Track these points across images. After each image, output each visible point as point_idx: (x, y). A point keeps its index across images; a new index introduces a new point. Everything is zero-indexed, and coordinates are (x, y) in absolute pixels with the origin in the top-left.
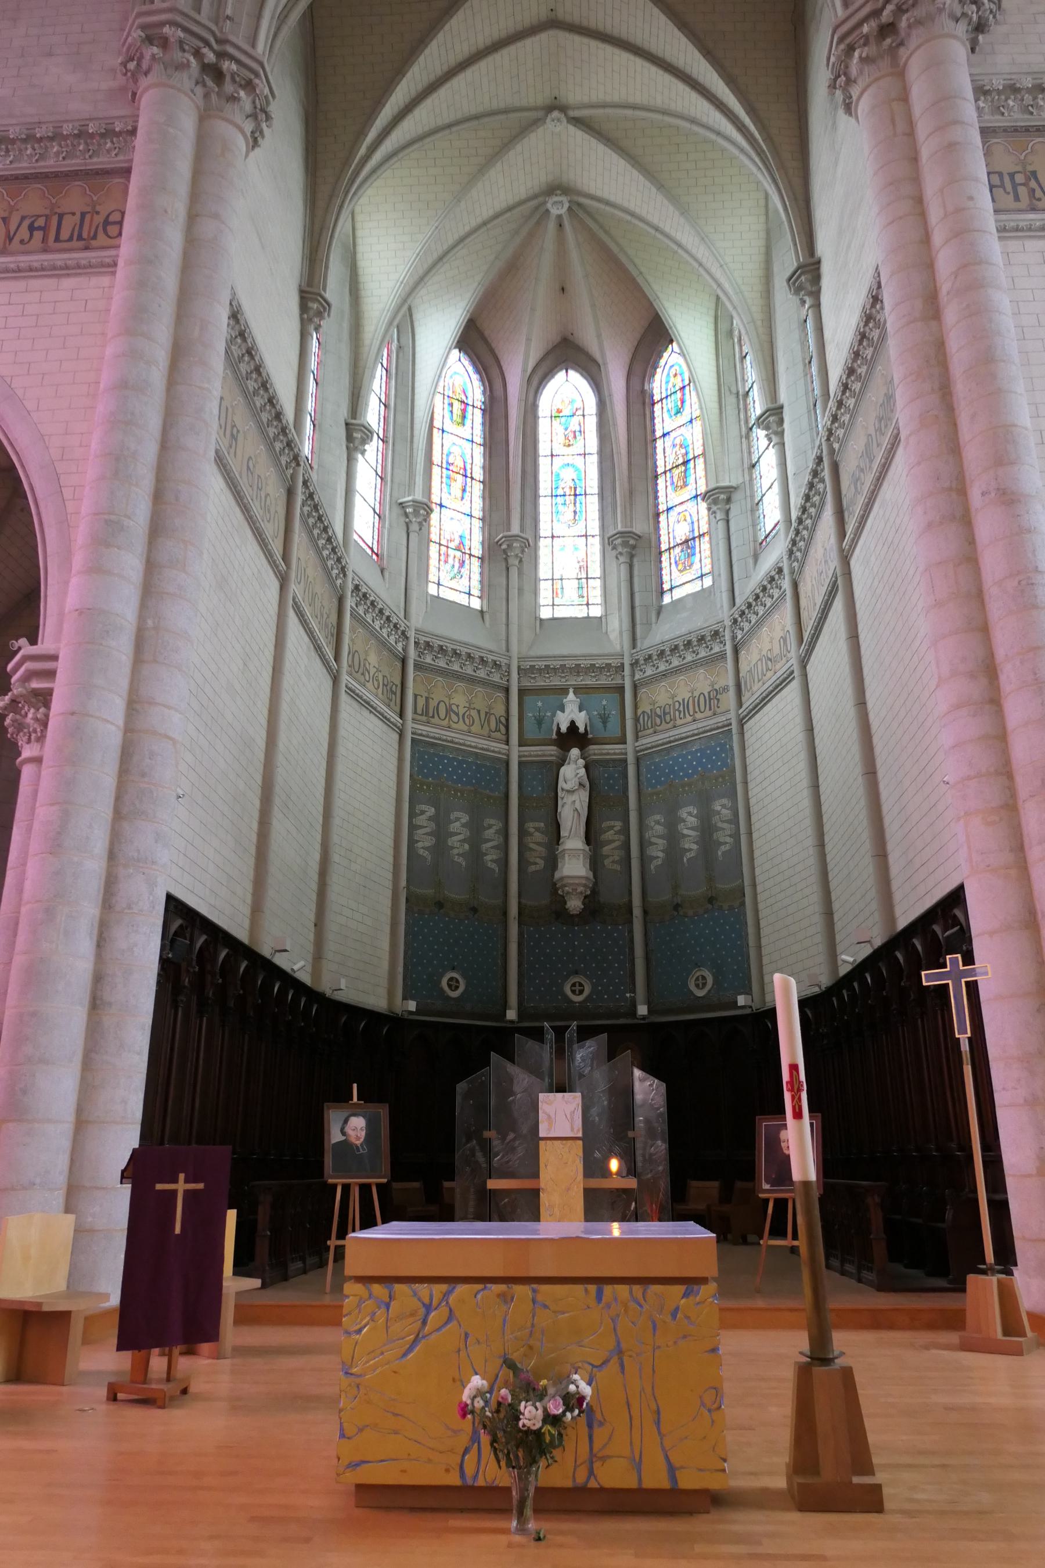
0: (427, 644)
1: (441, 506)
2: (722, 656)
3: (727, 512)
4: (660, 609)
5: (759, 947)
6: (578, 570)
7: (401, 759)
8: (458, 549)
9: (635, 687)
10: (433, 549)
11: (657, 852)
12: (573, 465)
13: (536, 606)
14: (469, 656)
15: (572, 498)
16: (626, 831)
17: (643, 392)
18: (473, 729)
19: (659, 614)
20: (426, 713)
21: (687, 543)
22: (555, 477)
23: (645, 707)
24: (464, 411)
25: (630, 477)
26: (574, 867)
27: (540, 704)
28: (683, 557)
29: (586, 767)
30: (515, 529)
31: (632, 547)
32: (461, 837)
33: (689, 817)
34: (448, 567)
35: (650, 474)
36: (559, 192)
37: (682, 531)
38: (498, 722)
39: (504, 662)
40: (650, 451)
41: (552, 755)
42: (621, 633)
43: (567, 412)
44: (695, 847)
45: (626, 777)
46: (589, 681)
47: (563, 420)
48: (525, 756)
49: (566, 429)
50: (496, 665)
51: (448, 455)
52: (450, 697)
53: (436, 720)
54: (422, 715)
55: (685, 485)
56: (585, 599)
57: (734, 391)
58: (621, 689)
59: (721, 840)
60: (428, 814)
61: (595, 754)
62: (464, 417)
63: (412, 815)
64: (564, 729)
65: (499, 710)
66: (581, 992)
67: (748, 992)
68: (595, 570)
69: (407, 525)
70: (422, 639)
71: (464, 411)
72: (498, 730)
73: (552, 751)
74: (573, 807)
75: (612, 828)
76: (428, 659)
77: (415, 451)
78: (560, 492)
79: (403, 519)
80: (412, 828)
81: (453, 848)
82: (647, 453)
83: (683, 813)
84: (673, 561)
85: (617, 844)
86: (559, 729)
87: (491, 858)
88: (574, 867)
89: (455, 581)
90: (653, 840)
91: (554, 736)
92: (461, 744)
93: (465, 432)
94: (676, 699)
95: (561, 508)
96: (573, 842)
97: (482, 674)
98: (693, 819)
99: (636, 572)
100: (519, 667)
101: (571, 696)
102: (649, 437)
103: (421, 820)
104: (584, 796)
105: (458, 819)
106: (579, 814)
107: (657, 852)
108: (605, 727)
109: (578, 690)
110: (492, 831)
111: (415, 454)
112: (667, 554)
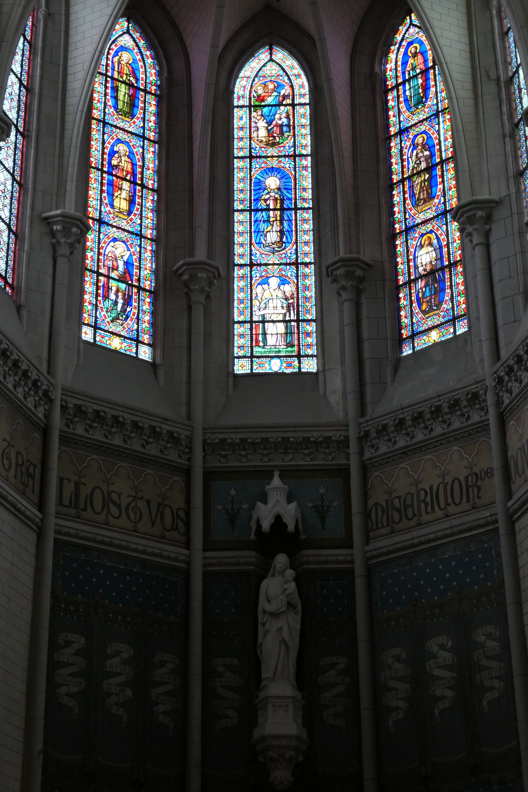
1: (101, 222)
2: (484, 427)
3: (487, 234)
4: (398, 362)
7: (39, 570)
8: (121, 280)
10: (89, 279)
13: (230, 358)
14: (135, 424)
19: (396, 369)
21: (435, 275)
22: (259, 186)
23: (378, 497)
25: (355, 188)
27: (233, 492)
29: (297, 580)
30: (201, 254)
31: (357, 278)
33: (441, 650)
34: (108, 304)
37: (426, 257)
46: (301, 461)
47: (266, 110)
49: (269, 123)
50: (174, 439)
54: (69, 506)
56: (296, 348)
57: (493, 76)
63: (53, 647)
64: (266, 526)
65: (177, 500)
69: (54, 247)
70: (72, 402)
72: (175, 528)
73: (249, 556)
74: (278, 637)
76: (80, 430)
77: (66, 149)
79: (47, 240)
80: (53, 666)
83: (433, 645)
88: (280, 723)
91: (253, 537)
92: (123, 548)
94: (420, 486)
95: (262, 226)
96: (280, 686)
97: (153, 450)
99: (364, 312)
100: (204, 441)
101: (276, 481)
102: (381, 135)
105: (117, 653)
106: (287, 647)
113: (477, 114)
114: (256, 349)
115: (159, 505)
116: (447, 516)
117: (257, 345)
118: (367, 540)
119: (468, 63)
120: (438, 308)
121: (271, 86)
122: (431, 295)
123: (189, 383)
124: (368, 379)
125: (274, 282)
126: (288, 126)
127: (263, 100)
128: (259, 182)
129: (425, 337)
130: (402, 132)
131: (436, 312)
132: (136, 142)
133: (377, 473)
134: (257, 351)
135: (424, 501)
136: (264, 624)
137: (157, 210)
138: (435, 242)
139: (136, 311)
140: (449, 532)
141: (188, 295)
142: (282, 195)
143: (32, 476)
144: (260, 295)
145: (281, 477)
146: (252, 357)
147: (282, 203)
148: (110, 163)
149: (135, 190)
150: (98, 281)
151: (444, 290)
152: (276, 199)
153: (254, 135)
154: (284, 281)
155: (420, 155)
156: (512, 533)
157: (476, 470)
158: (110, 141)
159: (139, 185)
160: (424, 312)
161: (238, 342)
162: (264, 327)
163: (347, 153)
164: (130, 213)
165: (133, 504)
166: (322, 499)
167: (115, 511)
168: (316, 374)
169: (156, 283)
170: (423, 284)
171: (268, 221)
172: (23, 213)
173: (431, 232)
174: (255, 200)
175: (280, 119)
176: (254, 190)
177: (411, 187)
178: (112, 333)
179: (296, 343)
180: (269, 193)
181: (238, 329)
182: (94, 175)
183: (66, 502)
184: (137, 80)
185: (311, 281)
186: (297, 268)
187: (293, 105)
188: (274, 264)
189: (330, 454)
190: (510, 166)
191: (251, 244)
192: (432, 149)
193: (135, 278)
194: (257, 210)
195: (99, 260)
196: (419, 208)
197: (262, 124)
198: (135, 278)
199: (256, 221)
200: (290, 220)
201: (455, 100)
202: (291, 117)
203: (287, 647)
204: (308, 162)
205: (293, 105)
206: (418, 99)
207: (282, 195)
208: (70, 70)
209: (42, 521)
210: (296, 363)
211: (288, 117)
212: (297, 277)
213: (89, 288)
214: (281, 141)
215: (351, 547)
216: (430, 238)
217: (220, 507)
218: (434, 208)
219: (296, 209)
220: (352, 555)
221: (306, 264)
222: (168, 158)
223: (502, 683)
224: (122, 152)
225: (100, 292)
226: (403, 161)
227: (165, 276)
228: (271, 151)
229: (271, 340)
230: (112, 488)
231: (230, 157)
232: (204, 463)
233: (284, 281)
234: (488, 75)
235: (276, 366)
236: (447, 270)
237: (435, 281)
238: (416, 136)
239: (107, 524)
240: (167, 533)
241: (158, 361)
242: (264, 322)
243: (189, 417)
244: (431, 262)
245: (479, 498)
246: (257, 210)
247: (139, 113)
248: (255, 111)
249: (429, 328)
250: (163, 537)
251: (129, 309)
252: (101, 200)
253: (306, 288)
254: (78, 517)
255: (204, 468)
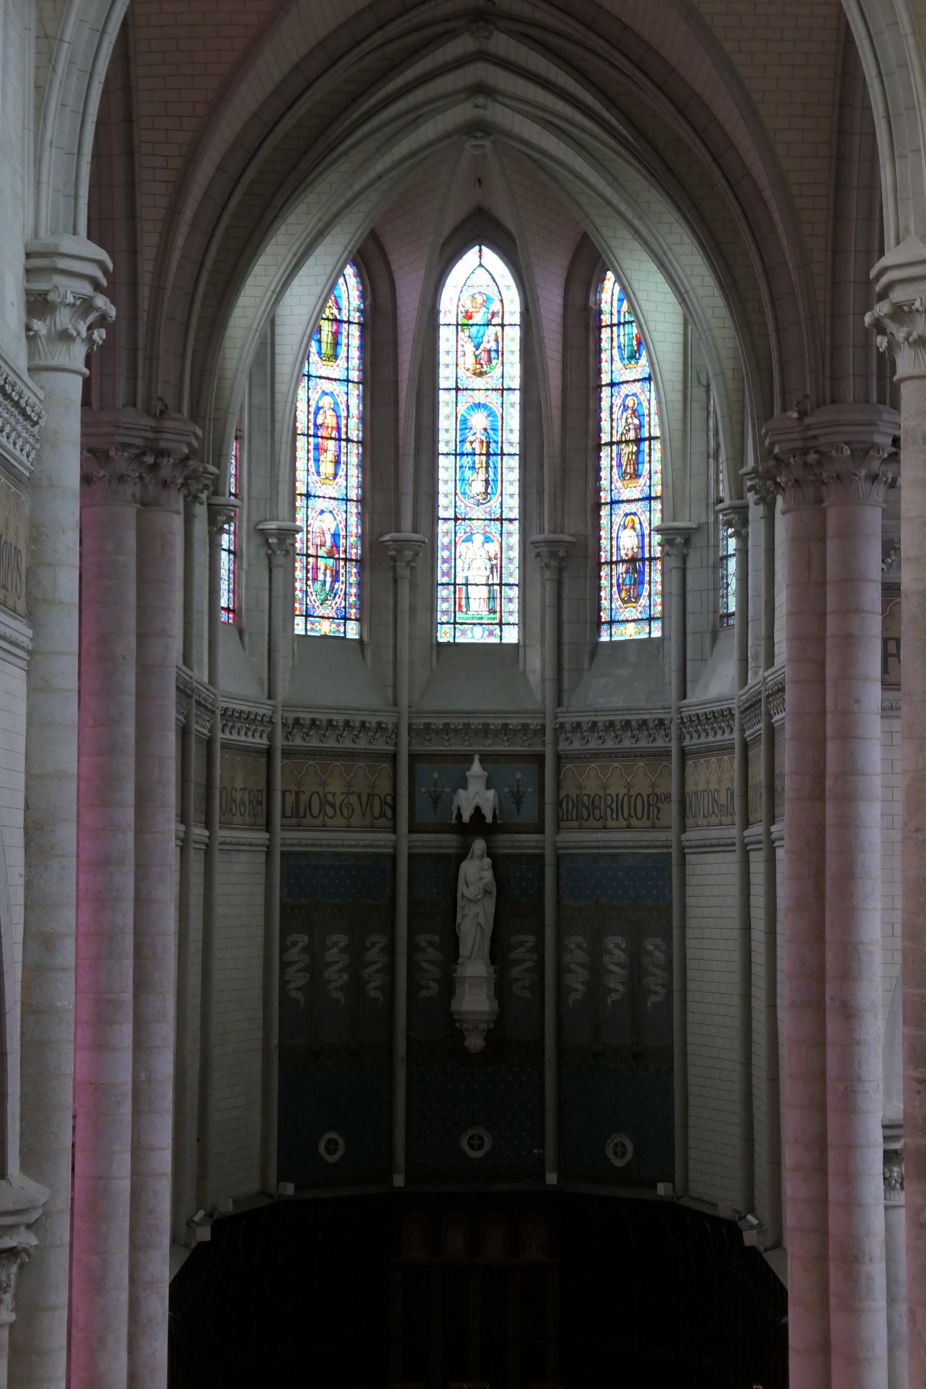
0: (297, 721)
1: (308, 496)
2: (668, 754)
3: (684, 559)
4: (597, 645)
5: (686, 1126)
6: (488, 572)
7: (269, 886)
8: (330, 556)
9: (559, 758)
11: (577, 980)
12: (485, 406)
13: (433, 624)
14: (347, 723)
15: (484, 458)
16: (539, 948)
17: (586, 308)
18: (354, 821)
19: (593, 654)
20: (297, 816)
21: (635, 562)
22: (464, 425)
23: (569, 789)
24: (336, 334)
25: (563, 449)
26: (475, 1000)
27: (436, 775)
28: (627, 582)
29: (494, 867)
31: (562, 556)
32: (339, 966)
33: (616, 948)
34: (318, 585)
35: (591, 443)
36: (479, 134)
37: (628, 542)
38: (383, 803)
39: (388, 720)
40: (592, 406)
41: (451, 847)
42: (543, 679)
43: (479, 317)
44: (621, 988)
45: (542, 877)
46: (502, 747)
47: (474, 330)
48: (416, 847)
49: (477, 347)
51: (316, 414)
52: (324, 784)
53: (309, 820)
54: (291, 817)
55: (636, 475)
56: (498, 615)
57: (704, 382)
58: (539, 758)
59: (652, 987)
60: (300, 945)
61: (504, 847)
62: (336, 344)
63: (283, 950)
64: (466, 818)
65: (384, 787)
66: (480, 1147)
67: (672, 1180)
68: (512, 573)
69: (269, 558)
71: (336, 334)
72: (383, 815)
73: (449, 842)
74: (475, 919)
75: (521, 944)
76: (298, 741)
77: (277, 444)
78: (467, 448)
79: (263, 552)
80: (284, 965)
81: (329, 982)
82: (587, 409)
84: (614, 581)
85: (528, 964)
86: (459, 816)
87: (373, 989)
88: (475, 1000)
89: (325, 609)
90: (573, 967)
91: (454, 821)
92: (337, 846)
93: (336, 370)
94: (608, 792)
95: (468, 473)
96: (475, 968)
97: (362, 744)
98: (621, 953)
99: (565, 594)
100: (410, 725)
101: (476, 767)
102: (592, 384)
103: (293, 954)
104: (490, 906)
105: (335, 944)
106: (483, 930)
107: (577, 980)
108: (519, 809)
109: (485, 758)
110: (375, 950)
111: (277, 450)
112: (608, 507)
113: (684, 432)
114: (458, 614)
115: (369, 795)
116: (629, 827)
117: (460, 610)
118: (558, 829)
119: (680, 358)
120: (636, 602)
121: (480, 299)
122: (631, 585)
123: (395, 664)
124: (566, 666)
125: (478, 539)
126: (497, 351)
127: (470, 318)
128: (465, 421)
129: (622, 628)
130: (612, 384)
131: (634, 605)
132: (339, 388)
133: (570, 766)
134: (461, 617)
135: (610, 806)
136: (463, 907)
137: (362, 466)
138: (638, 526)
139: (343, 587)
140: (630, 844)
141: (394, 569)
142: (488, 437)
143: (259, 803)
144: (463, 554)
145: (481, 761)
146: (455, 623)
147: (488, 447)
148: (315, 424)
149: (340, 446)
150: (308, 563)
151: (642, 583)
152: (482, 442)
153: (460, 361)
154: (487, 540)
155: (630, 420)
156: (683, 864)
157: (657, 791)
158: (314, 396)
159: (344, 440)
160: (622, 600)
161: (442, 606)
162: (467, 590)
163: (556, 413)
164: (335, 475)
165: (346, 801)
166: (518, 785)
167: (329, 810)
168: (516, 646)
169: (362, 550)
170: (624, 570)
171: (474, 468)
172: (240, 528)
173: (635, 514)
174: (461, 430)
175: (489, 342)
176: (461, 430)
177: (619, 455)
178: (323, 617)
179: (498, 609)
180: (475, 434)
181: (442, 592)
182: (301, 442)
183: (288, 813)
184: (340, 309)
185: (515, 540)
186: (502, 524)
187: (502, 325)
188: (478, 519)
189: (527, 740)
190: (712, 492)
191: (456, 494)
192: (641, 418)
193: (342, 549)
194: (462, 454)
195: (308, 540)
196: (626, 482)
197: (469, 348)
198: (342, 549)
199: (461, 467)
200: (495, 468)
201: (664, 405)
202: (500, 340)
203: (483, 930)
204: (515, 397)
205: (502, 325)
206: (631, 352)
207: (488, 437)
208: (278, 350)
209: (269, 840)
210: (498, 632)
211: (496, 340)
212: (501, 534)
213: (299, 574)
214: (489, 370)
215: (541, 831)
216: (633, 521)
217: (424, 790)
218: (640, 489)
219: (502, 454)
220: (543, 842)
221: (511, 520)
222: (372, 405)
223: (664, 991)
224: (327, 406)
225: (310, 575)
226: (612, 420)
227: (371, 545)
228: (479, 383)
229: (474, 605)
230: (328, 789)
231: (434, 388)
232: (409, 746)
233: (487, 540)
234: (699, 379)
235: (477, 636)
236: (647, 563)
237: (635, 570)
238: (627, 396)
239: (324, 826)
240: (375, 821)
241: (366, 638)
242: (467, 585)
243: (395, 703)
244: (633, 548)
245: (658, 819)
246: (462, 454)
247: (342, 351)
248: (462, 331)
249: (631, 619)
250: (372, 827)
251: (336, 586)
252: (308, 470)
253: (510, 548)
254: (299, 825)
255: (409, 750)
